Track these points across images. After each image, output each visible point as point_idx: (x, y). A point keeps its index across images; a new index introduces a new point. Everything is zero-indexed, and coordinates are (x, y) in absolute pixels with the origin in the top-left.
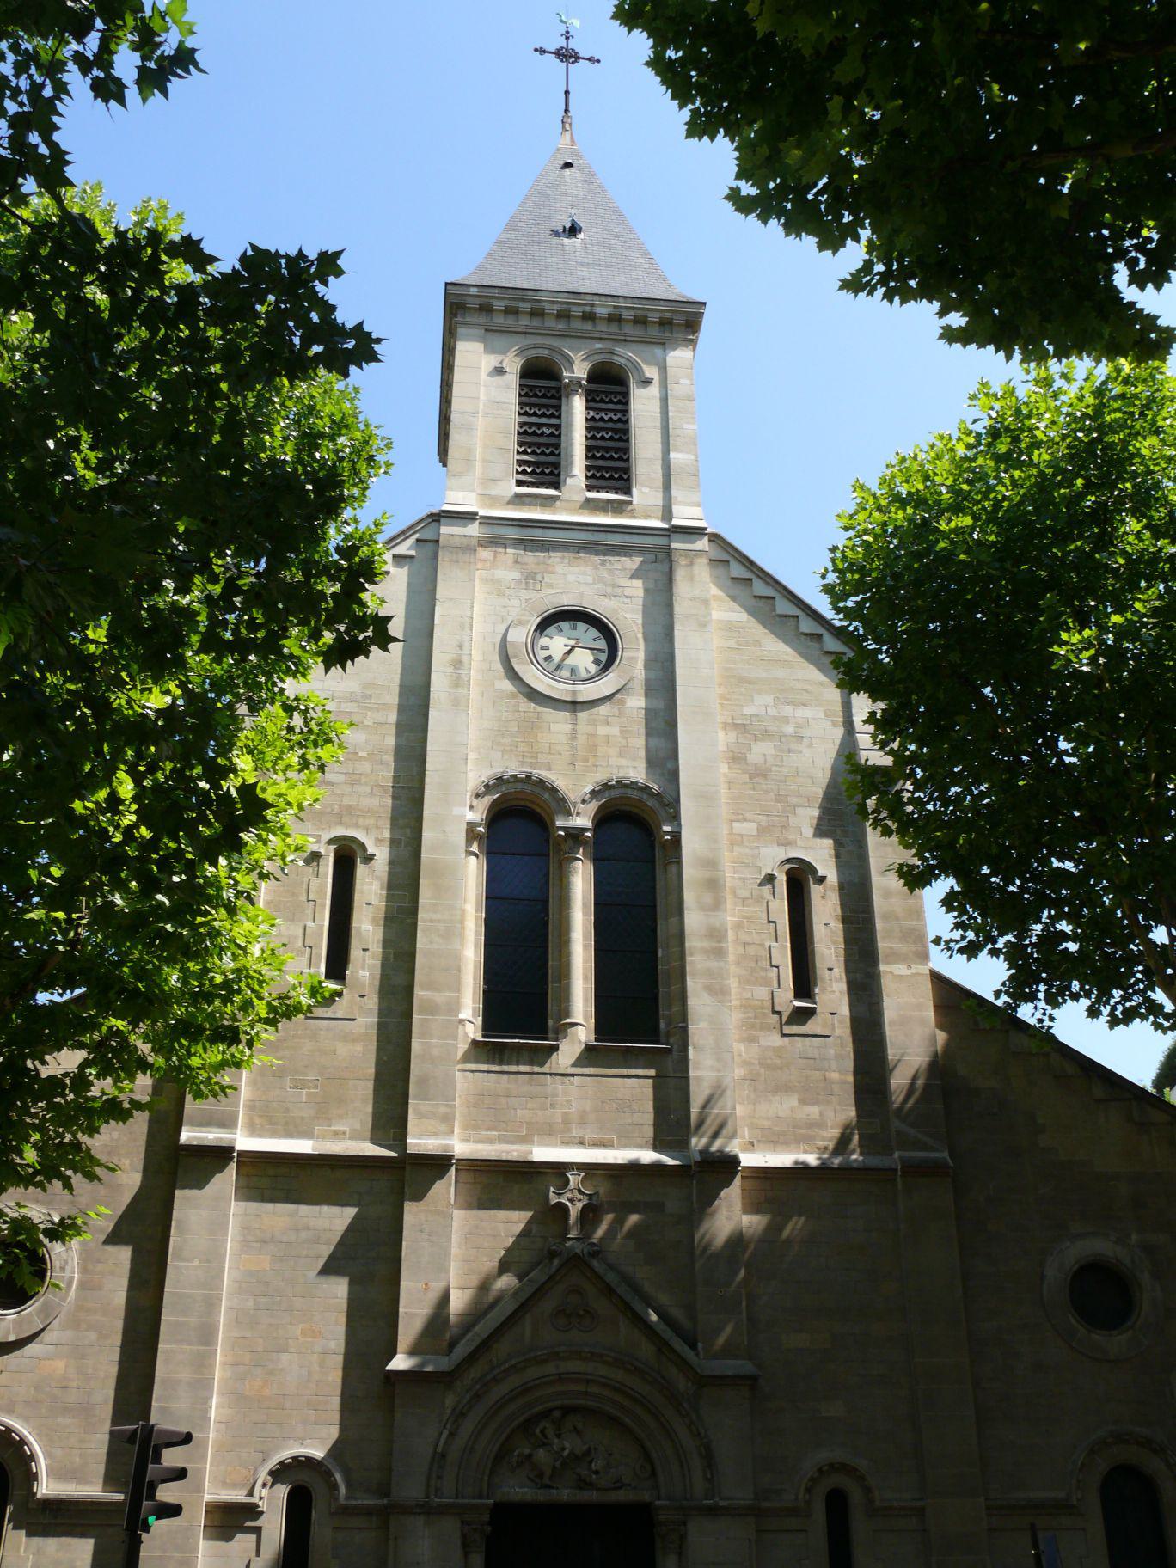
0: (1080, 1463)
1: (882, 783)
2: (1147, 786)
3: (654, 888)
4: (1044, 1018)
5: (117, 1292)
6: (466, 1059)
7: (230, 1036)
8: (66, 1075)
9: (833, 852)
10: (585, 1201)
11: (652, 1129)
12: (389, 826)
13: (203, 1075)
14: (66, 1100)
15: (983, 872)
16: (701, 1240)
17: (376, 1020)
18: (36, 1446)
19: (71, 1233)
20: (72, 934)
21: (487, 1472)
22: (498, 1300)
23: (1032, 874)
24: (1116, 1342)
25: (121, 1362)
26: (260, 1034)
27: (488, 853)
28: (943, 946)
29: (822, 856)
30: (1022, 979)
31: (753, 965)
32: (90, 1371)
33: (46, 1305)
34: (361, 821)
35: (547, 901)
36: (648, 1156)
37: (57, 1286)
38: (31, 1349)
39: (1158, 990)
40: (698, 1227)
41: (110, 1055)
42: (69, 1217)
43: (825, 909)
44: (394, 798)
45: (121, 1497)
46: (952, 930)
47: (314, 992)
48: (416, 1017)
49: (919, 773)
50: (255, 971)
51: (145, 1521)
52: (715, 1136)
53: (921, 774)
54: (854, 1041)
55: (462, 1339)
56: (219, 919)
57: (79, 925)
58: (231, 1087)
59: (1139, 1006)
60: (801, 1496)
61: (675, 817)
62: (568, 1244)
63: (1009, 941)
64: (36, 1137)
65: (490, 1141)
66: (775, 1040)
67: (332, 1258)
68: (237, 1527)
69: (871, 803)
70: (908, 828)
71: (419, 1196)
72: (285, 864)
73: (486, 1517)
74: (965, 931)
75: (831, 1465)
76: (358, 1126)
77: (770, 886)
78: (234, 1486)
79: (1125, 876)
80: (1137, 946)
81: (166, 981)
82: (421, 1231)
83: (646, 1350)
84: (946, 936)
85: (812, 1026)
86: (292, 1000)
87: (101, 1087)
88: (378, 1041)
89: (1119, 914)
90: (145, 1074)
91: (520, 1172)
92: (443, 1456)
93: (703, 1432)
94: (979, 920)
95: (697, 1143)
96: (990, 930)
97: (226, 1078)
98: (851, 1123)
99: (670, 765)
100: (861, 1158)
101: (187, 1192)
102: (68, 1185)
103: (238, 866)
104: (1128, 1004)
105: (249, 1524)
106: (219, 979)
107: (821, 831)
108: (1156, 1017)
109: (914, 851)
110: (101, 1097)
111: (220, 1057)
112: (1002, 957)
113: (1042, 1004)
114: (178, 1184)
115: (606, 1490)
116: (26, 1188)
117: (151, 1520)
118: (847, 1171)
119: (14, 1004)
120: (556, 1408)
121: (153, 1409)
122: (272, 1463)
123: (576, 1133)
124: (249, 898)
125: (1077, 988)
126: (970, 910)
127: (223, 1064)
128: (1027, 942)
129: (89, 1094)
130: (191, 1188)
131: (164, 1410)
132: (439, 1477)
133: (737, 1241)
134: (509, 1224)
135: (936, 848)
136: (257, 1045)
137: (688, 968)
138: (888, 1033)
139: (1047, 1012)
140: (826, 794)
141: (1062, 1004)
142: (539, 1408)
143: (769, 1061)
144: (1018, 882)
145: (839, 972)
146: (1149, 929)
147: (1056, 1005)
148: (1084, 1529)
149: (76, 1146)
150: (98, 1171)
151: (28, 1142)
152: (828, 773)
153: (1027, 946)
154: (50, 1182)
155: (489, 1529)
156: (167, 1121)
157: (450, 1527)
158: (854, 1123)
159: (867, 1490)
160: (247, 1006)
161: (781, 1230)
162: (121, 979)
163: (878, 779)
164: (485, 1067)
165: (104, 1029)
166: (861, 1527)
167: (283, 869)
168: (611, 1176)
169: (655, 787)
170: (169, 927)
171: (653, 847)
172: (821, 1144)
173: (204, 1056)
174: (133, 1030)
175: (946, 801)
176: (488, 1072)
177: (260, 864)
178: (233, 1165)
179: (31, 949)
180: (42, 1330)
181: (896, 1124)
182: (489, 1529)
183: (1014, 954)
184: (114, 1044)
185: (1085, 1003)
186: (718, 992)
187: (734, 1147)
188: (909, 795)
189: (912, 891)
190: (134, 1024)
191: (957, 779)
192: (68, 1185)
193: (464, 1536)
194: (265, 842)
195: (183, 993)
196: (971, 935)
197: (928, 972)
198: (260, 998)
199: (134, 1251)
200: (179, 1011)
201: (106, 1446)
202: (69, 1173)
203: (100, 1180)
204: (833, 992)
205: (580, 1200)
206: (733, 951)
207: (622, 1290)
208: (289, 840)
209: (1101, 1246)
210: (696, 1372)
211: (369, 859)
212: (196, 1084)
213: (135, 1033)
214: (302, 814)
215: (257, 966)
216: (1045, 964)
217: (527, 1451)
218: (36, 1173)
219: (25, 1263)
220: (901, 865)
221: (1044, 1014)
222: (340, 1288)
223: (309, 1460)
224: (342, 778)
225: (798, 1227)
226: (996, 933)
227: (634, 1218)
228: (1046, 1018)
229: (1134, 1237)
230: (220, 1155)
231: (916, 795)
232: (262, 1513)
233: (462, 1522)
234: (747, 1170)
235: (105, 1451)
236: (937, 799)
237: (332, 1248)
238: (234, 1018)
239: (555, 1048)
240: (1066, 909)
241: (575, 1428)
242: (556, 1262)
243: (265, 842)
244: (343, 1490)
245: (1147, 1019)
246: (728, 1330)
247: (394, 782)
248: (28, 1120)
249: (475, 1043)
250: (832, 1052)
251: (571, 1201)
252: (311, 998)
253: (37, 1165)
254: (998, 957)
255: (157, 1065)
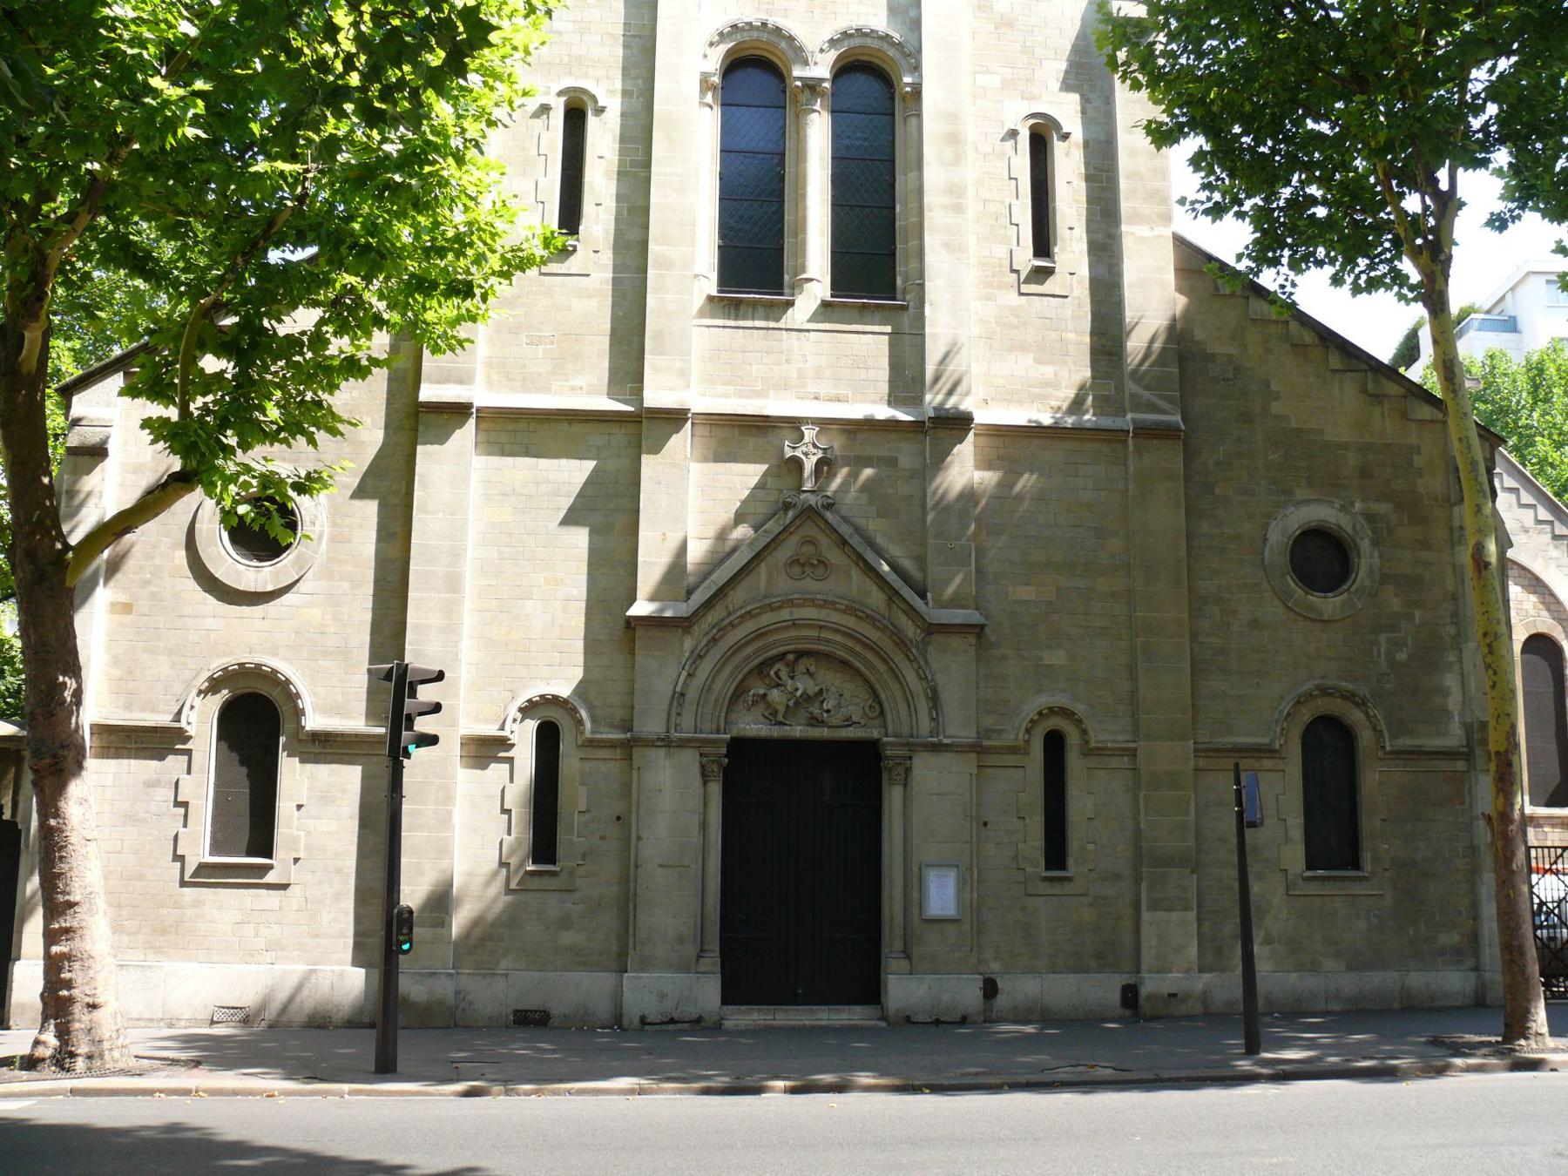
0: (1285, 713)
1: (1134, 34)
2: (1415, 43)
3: (893, 142)
4: (1286, 283)
5: (365, 542)
6: (702, 314)
7: (464, 290)
8: (303, 333)
9: (1079, 108)
10: (820, 455)
11: (887, 385)
12: (620, 77)
13: (439, 330)
14: (305, 359)
15: (1234, 131)
16: (935, 493)
17: (611, 275)
18: (300, 684)
19: (317, 486)
20: (299, 189)
21: (725, 708)
22: (734, 550)
23: (1285, 136)
24: (1330, 604)
25: (374, 610)
26: (495, 288)
27: (722, 105)
28: (1187, 206)
29: (1067, 111)
30: (1266, 242)
31: (993, 222)
32: (346, 618)
33: (299, 557)
34: (591, 72)
35: (783, 154)
36: (883, 412)
37: (308, 537)
38: (287, 598)
39: (1405, 258)
40: (930, 484)
41: (345, 314)
42: (315, 471)
43: (1068, 165)
44: (625, 47)
45: (382, 730)
46: (1198, 191)
47: (547, 243)
48: (650, 272)
49: (1174, 24)
50: (486, 224)
51: (406, 749)
52: (950, 393)
53: (1176, 24)
54: (1093, 302)
55: (699, 586)
56: (448, 168)
57: (305, 179)
58: (468, 340)
59: (1385, 275)
60: (1021, 736)
61: (917, 68)
62: (803, 496)
63: (1256, 204)
64: (278, 394)
65: (726, 396)
66: (1012, 298)
67: (571, 509)
68: (489, 757)
69: (1122, 55)
70: (1158, 80)
71: (656, 450)
72: (513, 110)
73: (724, 751)
74: (1212, 192)
75: (1051, 709)
76: (595, 381)
77: (1013, 141)
78: (486, 721)
79: (1382, 137)
80: (1388, 214)
81: (398, 237)
82: (659, 484)
83: (877, 598)
84: (1191, 197)
85: (1050, 286)
86: (525, 253)
87: (339, 346)
88: (613, 297)
89: (1372, 180)
90: (381, 330)
91: (754, 426)
92: (682, 695)
93: (930, 677)
94: (1227, 182)
95: (932, 399)
96: (1238, 192)
97: (462, 331)
98: (1085, 384)
99: (912, 13)
100: (1094, 418)
101: (429, 447)
102: (312, 441)
103: (464, 113)
104: (1373, 274)
105: (502, 754)
106: (450, 234)
107: (1067, 86)
108: (1401, 287)
109: (1163, 107)
110: (339, 355)
111: (455, 312)
112: (1248, 220)
113: (1284, 270)
114: (419, 440)
115: (836, 727)
116: (272, 445)
117: (411, 748)
118: (1078, 432)
119: (247, 262)
120: (789, 652)
121: (406, 652)
122: (521, 700)
123: (812, 388)
124: (477, 145)
125: (1322, 255)
126: (1218, 171)
127: (458, 320)
128: (1275, 205)
129: (327, 353)
130: (432, 443)
131: (417, 653)
132: (679, 714)
133: (969, 496)
134: (746, 476)
135: (1187, 104)
136: (491, 299)
137: (926, 225)
138: (1126, 295)
139: (1290, 279)
140: (1074, 46)
141: (1305, 270)
142: (775, 651)
143: (1005, 320)
144: (1270, 143)
145: (1081, 232)
146: (1402, 196)
147: (1299, 271)
148: (1283, 771)
149: (318, 404)
150: (340, 427)
151: (270, 400)
152: (1078, 24)
153: (1274, 210)
154: (295, 439)
155: (727, 760)
156: (406, 380)
157: (690, 760)
158: (1088, 384)
159: (1084, 732)
160: (479, 259)
161: (1011, 487)
162: (352, 232)
163: (1130, 30)
164: (720, 322)
165: (338, 285)
166: (1075, 764)
167: (510, 116)
168: (846, 431)
169: (897, 36)
170: (398, 178)
171: (893, 99)
172: (1056, 404)
173: (439, 310)
174: (367, 286)
175: (1200, 55)
176: (724, 327)
177: (488, 111)
178: (472, 421)
179: (258, 206)
180: (297, 581)
181: (1131, 387)
182: (727, 760)
183: (1261, 218)
184: (348, 301)
185: (1329, 270)
186: (955, 248)
187: (967, 405)
188: (1162, 47)
189: (1159, 149)
190: (368, 279)
191: (1213, 32)
192: (312, 441)
193: (703, 767)
194: (492, 89)
195: (416, 249)
196: (1217, 197)
197: (1171, 235)
198: (493, 251)
199: (380, 505)
200: (412, 266)
201: (366, 686)
202: (313, 429)
203: (342, 435)
204: (1072, 250)
205: (814, 454)
206: (972, 207)
207: (855, 541)
208: (515, 86)
209: (1324, 513)
210: (925, 620)
211: (600, 111)
212: (433, 339)
213: (369, 290)
214: (529, 59)
215: (489, 219)
216: (1292, 230)
217: (762, 691)
218: (280, 429)
219: (275, 515)
220: (1150, 122)
221: (1286, 280)
222: (580, 538)
223: (555, 698)
224: (570, 26)
225: (1030, 484)
226: (1243, 196)
227: (868, 472)
228: (1288, 284)
229: (1358, 506)
230: (458, 412)
231: (1169, 48)
232: (513, 745)
233: (701, 755)
234: (980, 427)
235: (365, 690)
236: (1190, 53)
237: (572, 500)
238: (468, 272)
239: (790, 304)
240: (1317, 173)
241: (808, 670)
242: (791, 514)
243: (492, 89)
244: (588, 725)
245: (1392, 289)
246: (958, 580)
247: (625, 30)
248: (269, 377)
249: (710, 298)
250: (1069, 312)
251: (806, 454)
252: (544, 249)
253: (280, 421)
254: (1244, 220)
255: (393, 321)
